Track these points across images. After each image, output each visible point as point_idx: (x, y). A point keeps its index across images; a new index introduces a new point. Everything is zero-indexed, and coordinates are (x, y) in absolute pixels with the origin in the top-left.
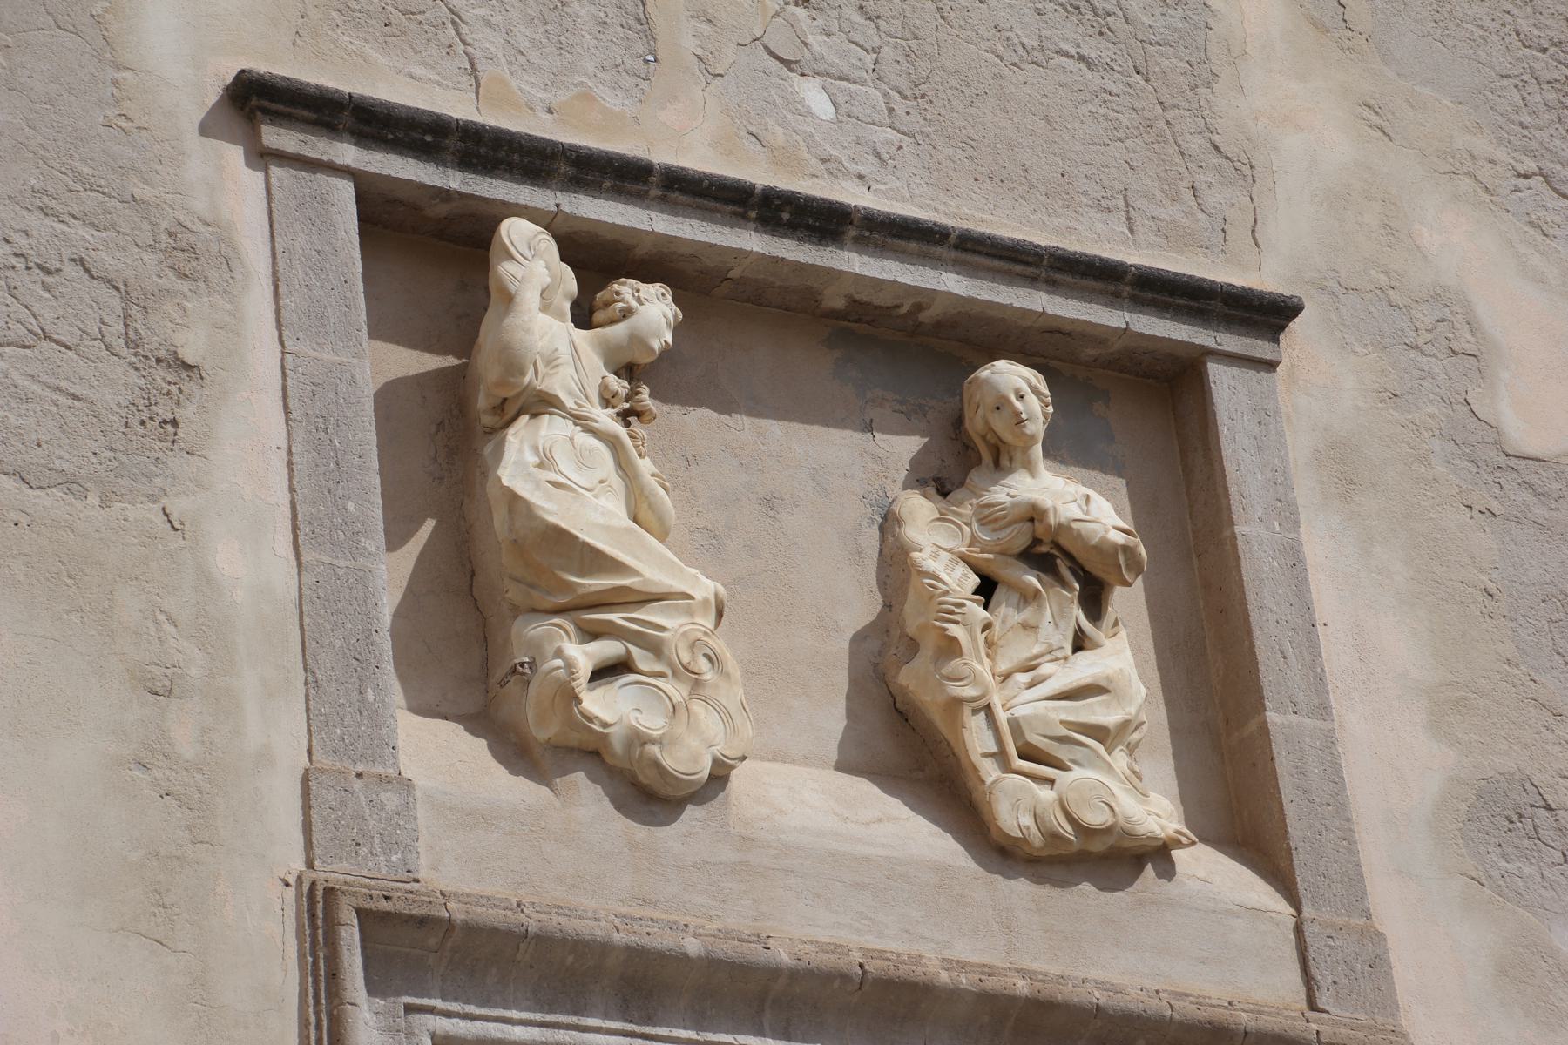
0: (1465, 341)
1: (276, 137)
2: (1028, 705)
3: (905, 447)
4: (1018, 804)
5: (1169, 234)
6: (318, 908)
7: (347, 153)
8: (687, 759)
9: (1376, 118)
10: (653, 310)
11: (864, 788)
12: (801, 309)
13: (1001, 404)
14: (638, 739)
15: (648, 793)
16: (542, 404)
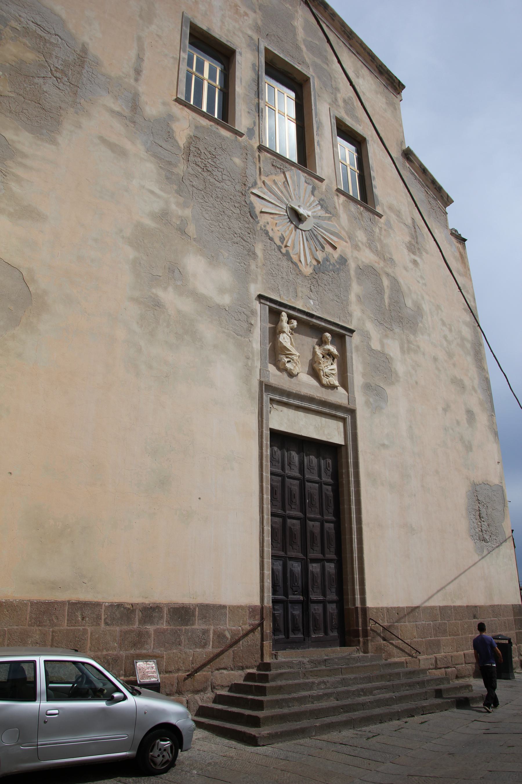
0: (369, 336)
1: (262, 301)
2: (326, 370)
3: (316, 340)
4: (325, 380)
5: (344, 321)
6: (261, 383)
7: (268, 303)
8: (295, 372)
9: (363, 311)
10: (295, 323)
11: (309, 376)
12: (311, 326)
13: (327, 338)
14: (291, 369)
15: (291, 375)
16: (284, 332)
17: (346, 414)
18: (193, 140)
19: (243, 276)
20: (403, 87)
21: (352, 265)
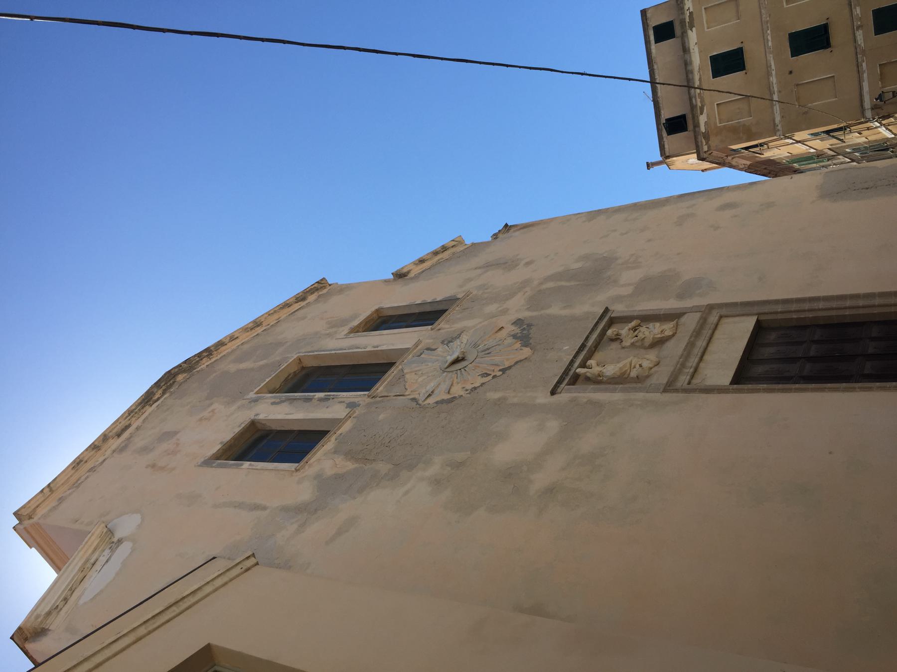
1: (559, 390)
7: (563, 386)
12: (588, 350)
17: (713, 316)
18: (350, 455)
19: (526, 410)
20: (324, 279)
21: (525, 314)
